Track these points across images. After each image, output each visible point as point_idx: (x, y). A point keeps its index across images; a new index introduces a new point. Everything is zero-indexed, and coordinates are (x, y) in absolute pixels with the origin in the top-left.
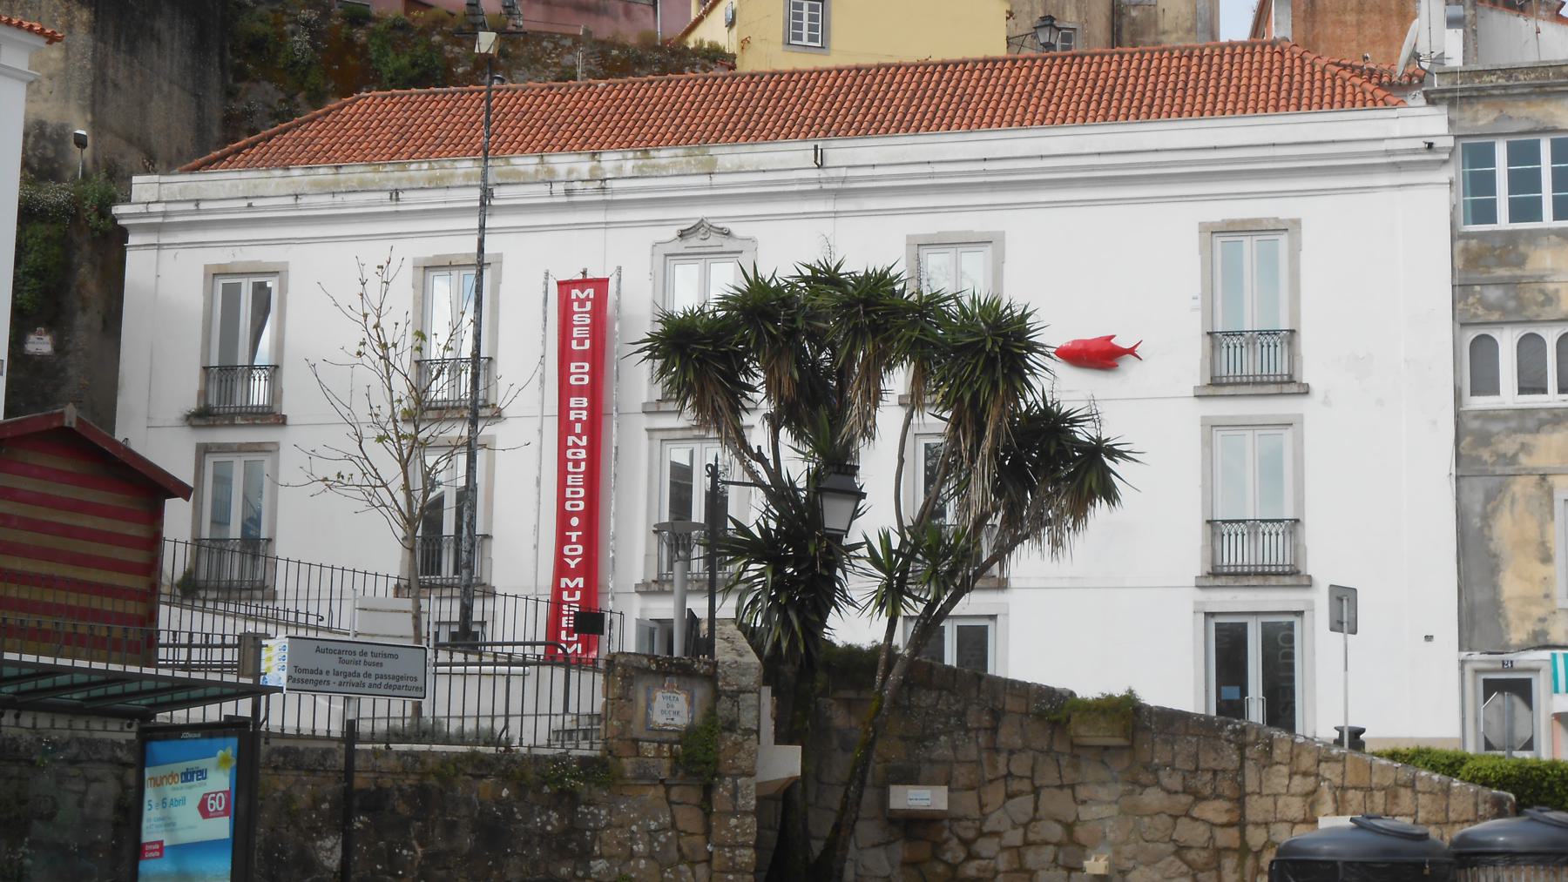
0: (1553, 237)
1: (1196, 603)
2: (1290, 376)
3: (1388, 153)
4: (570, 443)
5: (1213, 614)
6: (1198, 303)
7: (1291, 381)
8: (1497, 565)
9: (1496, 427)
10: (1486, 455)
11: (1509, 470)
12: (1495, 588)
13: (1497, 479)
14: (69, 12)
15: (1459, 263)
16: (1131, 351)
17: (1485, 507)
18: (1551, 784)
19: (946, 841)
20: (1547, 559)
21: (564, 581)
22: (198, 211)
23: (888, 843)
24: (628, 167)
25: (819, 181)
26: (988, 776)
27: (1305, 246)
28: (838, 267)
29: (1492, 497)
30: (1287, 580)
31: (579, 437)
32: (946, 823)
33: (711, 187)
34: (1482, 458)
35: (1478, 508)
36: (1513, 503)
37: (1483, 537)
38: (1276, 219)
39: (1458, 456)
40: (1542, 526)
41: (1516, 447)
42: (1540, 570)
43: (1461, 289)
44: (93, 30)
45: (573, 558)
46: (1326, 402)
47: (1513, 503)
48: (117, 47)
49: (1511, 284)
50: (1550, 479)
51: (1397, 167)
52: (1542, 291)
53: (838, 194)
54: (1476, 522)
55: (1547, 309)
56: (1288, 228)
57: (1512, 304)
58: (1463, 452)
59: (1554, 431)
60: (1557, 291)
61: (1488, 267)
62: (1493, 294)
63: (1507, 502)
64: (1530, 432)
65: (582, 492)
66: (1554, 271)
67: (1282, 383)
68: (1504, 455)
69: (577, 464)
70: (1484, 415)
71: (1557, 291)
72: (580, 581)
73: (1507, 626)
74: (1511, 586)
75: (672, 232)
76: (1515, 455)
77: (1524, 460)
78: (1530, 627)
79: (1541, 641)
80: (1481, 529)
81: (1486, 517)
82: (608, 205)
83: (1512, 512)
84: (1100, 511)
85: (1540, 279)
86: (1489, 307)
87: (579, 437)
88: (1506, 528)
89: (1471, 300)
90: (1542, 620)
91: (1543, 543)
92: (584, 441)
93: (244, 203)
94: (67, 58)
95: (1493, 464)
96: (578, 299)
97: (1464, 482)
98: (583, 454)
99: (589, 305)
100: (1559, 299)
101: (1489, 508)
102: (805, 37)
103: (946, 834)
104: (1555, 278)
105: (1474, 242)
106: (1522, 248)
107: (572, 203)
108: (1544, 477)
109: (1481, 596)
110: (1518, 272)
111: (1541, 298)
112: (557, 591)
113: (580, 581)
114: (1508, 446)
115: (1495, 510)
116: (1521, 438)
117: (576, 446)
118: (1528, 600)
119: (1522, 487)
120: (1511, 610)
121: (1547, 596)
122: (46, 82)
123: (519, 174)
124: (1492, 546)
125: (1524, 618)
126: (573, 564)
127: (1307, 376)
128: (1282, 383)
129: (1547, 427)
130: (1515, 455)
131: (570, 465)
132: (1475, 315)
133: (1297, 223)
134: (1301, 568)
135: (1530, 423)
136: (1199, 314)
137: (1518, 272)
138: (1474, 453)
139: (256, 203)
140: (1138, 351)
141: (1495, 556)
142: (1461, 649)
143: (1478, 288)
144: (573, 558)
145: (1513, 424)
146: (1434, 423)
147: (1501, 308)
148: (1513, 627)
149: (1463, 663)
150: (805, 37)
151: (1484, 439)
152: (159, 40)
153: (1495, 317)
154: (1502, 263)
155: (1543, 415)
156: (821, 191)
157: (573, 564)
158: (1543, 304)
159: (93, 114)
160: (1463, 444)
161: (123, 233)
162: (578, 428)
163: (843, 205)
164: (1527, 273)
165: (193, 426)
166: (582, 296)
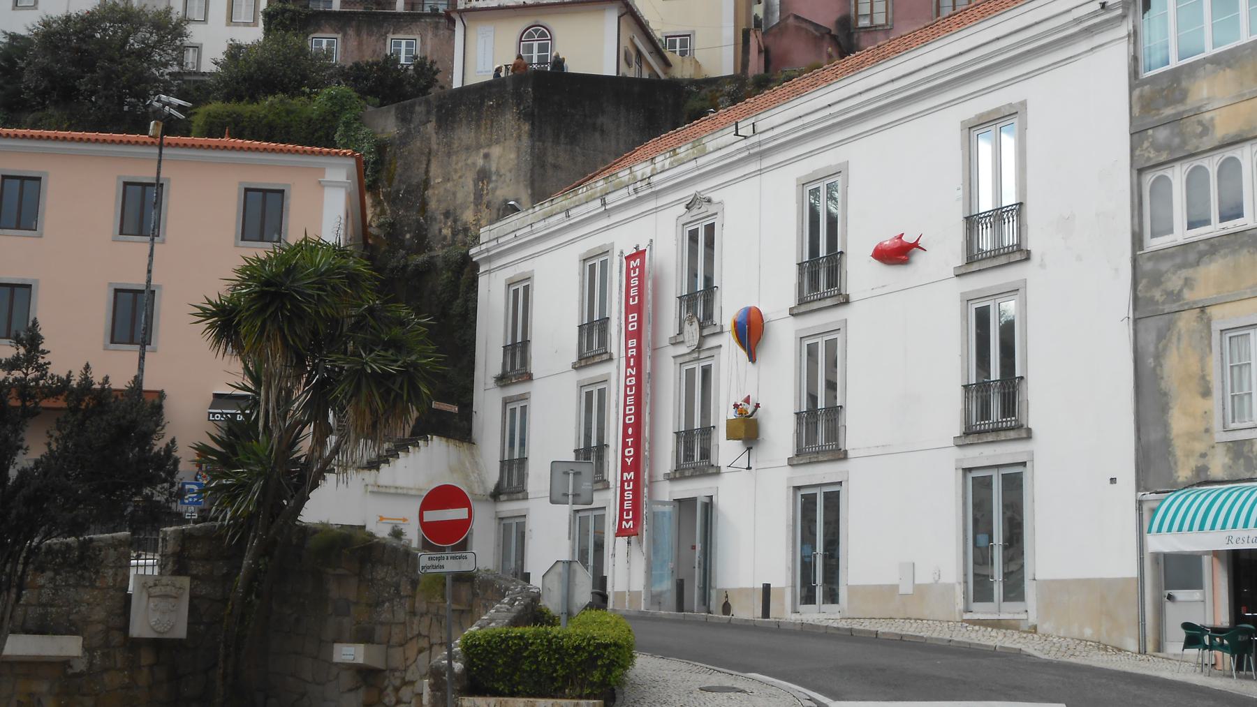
0: (1208, 66)
1: (957, 460)
2: (1019, 245)
3: (1078, 21)
5: (970, 470)
6: (960, 192)
7: (1020, 250)
8: (1167, 404)
9: (1165, 266)
10: (1158, 295)
11: (1175, 307)
12: (1166, 426)
13: (1166, 317)
14: (519, 127)
15: (1136, 111)
16: (916, 245)
17: (1157, 348)
18: (535, 653)
19: (386, 688)
20: (1206, 393)
21: (625, 474)
22: (499, 245)
23: (357, 688)
24: (667, 162)
25: (747, 148)
26: (409, 636)
27: (1029, 126)
29: (1162, 335)
30: (1012, 434)
32: (387, 673)
33: (698, 168)
34: (1156, 296)
35: (1152, 348)
36: (1179, 339)
37: (1157, 377)
38: (1010, 105)
39: (1136, 300)
40: (1202, 360)
41: (1181, 282)
42: (1200, 404)
43: (1137, 134)
44: (531, 136)
46: (1042, 266)
47: (1179, 339)
48: (556, 141)
49: (1176, 120)
50: (1208, 310)
51: (1089, 31)
52: (1200, 123)
53: (762, 155)
54: (1151, 362)
55: (1205, 139)
57: (1177, 141)
58: (1140, 295)
59: (1211, 261)
60: (1212, 119)
61: (1158, 109)
62: (1162, 134)
63: (1174, 339)
64: (1191, 266)
66: (1210, 99)
67: (1009, 253)
68: (1172, 292)
70: (1158, 255)
71: (1212, 119)
73: (1175, 463)
74: (1179, 423)
75: (681, 209)
76: (1181, 291)
77: (1188, 295)
78: (1193, 463)
79: (1203, 478)
80: (1154, 369)
81: (1158, 356)
82: (657, 194)
83: (1178, 349)
85: (1198, 111)
86: (1158, 149)
88: (1175, 365)
89: (1146, 144)
90: (1203, 455)
91: (1203, 377)
93: (512, 236)
94: (518, 156)
95: (1163, 303)
97: (1141, 325)
100: (1213, 126)
101: (1161, 346)
102: (404, 42)
103: (386, 682)
104: (1209, 107)
105: (1147, 88)
106: (1184, 84)
107: (639, 199)
108: (1203, 309)
109: (1154, 436)
110: (1181, 108)
111: (1200, 129)
112: (623, 482)
114: (1174, 282)
115: (1165, 349)
116: (1184, 273)
118: (1192, 436)
119: (1187, 321)
120: (1179, 447)
121: (1207, 431)
122: (508, 174)
123: (621, 183)
124: (1163, 385)
125: (1188, 454)
127: (1032, 244)
128: (1009, 253)
129: (1206, 259)
130: (1181, 291)
132: (1149, 159)
133: (1024, 104)
134: (1024, 422)
135: (1192, 257)
136: (961, 203)
137: (1181, 108)
138: (1148, 295)
139: (518, 233)
140: (921, 243)
141: (1165, 394)
142: (1138, 490)
143: (1150, 132)
145: (1178, 260)
146: (1117, 270)
147: (1168, 147)
148: (1180, 464)
149: (1140, 503)
150: (404, 42)
151: (1157, 279)
152: (602, 131)
153: (1164, 157)
154: (1169, 103)
155: (1202, 247)
156: (750, 156)
158: (1202, 135)
159: (533, 188)
160: (1140, 287)
161: (476, 266)
163: (767, 162)
164: (1188, 107)
165: (502, 386)
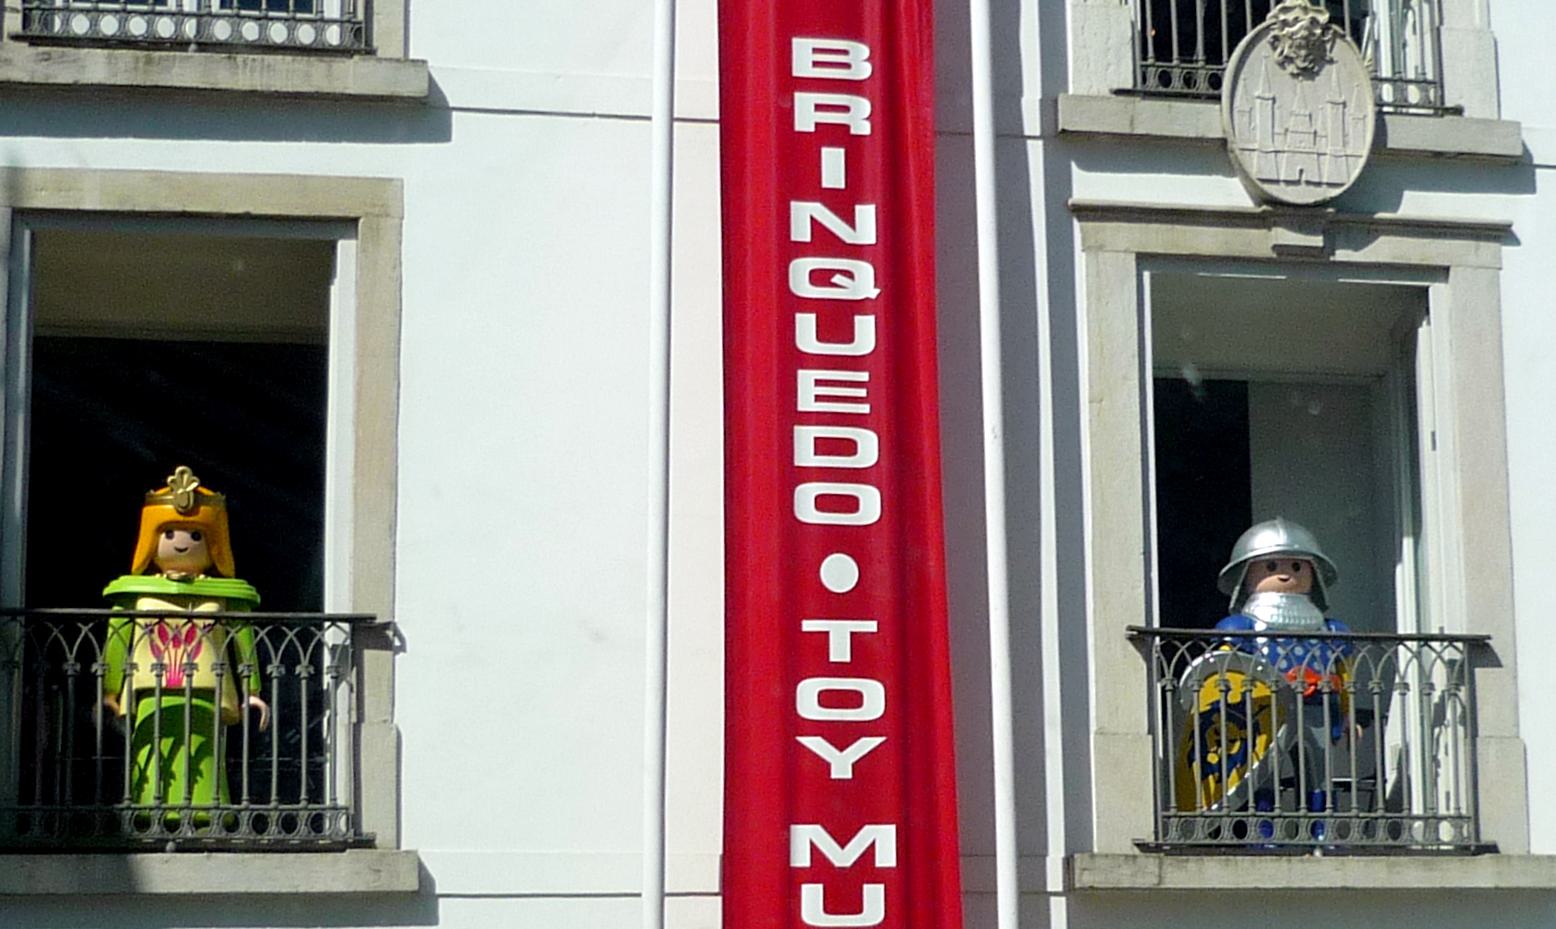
4: (801, 232)
28: (1278, 607)
31: (843, 204)
45: (841, 735)
56: (1500, 233)
65: (868, 448)
69: (836, 320)
72: (882, 841)
84: (1514, 228)
87: (843, 204)
92: (866, 225)
96: (820, 867)
98: (863, 282)
99: (866, 334)
113: (882, 841)
117: (824, 241)
126: (841, 764)
131: (806, 326)
144: (841, 735)
157: (841, 764)
162: (833, 167)
166: (843, 857)
